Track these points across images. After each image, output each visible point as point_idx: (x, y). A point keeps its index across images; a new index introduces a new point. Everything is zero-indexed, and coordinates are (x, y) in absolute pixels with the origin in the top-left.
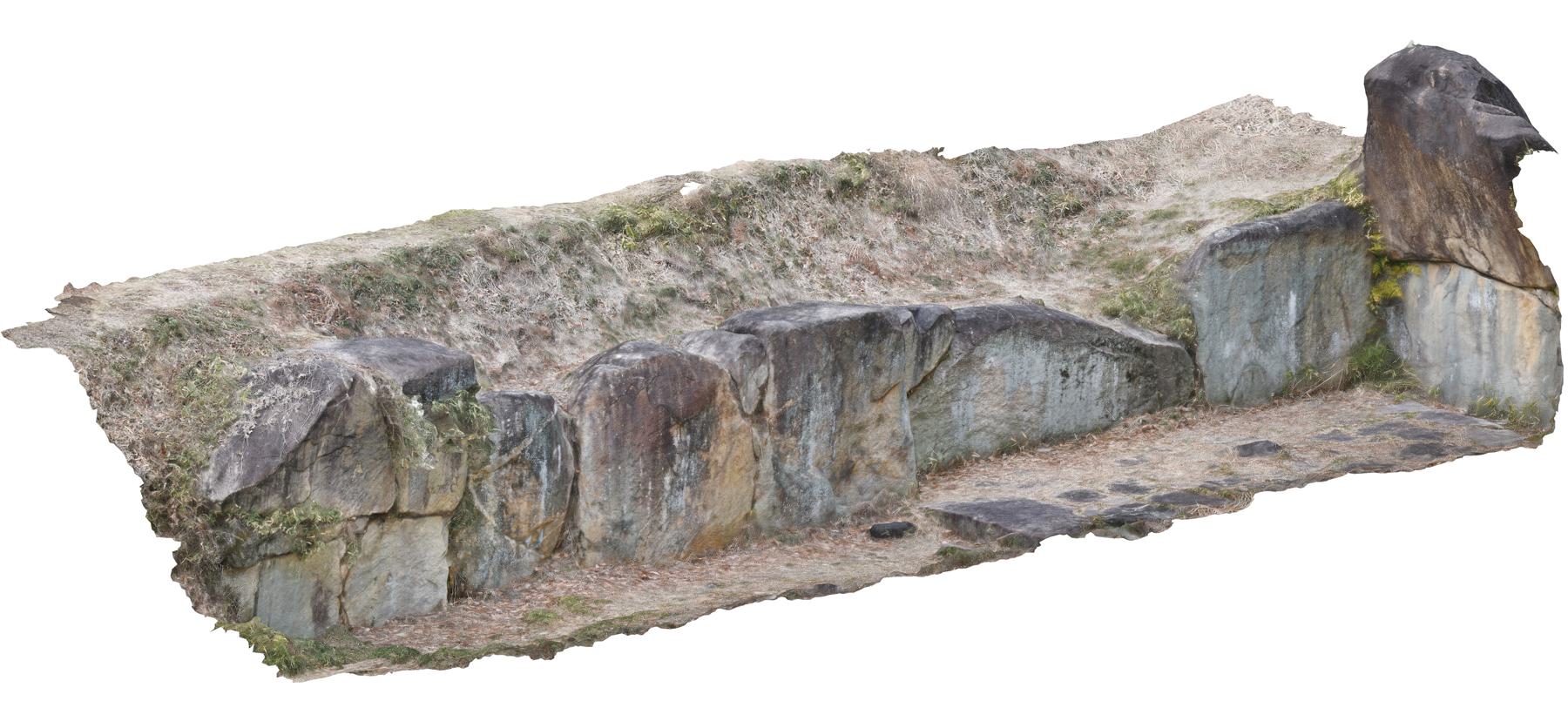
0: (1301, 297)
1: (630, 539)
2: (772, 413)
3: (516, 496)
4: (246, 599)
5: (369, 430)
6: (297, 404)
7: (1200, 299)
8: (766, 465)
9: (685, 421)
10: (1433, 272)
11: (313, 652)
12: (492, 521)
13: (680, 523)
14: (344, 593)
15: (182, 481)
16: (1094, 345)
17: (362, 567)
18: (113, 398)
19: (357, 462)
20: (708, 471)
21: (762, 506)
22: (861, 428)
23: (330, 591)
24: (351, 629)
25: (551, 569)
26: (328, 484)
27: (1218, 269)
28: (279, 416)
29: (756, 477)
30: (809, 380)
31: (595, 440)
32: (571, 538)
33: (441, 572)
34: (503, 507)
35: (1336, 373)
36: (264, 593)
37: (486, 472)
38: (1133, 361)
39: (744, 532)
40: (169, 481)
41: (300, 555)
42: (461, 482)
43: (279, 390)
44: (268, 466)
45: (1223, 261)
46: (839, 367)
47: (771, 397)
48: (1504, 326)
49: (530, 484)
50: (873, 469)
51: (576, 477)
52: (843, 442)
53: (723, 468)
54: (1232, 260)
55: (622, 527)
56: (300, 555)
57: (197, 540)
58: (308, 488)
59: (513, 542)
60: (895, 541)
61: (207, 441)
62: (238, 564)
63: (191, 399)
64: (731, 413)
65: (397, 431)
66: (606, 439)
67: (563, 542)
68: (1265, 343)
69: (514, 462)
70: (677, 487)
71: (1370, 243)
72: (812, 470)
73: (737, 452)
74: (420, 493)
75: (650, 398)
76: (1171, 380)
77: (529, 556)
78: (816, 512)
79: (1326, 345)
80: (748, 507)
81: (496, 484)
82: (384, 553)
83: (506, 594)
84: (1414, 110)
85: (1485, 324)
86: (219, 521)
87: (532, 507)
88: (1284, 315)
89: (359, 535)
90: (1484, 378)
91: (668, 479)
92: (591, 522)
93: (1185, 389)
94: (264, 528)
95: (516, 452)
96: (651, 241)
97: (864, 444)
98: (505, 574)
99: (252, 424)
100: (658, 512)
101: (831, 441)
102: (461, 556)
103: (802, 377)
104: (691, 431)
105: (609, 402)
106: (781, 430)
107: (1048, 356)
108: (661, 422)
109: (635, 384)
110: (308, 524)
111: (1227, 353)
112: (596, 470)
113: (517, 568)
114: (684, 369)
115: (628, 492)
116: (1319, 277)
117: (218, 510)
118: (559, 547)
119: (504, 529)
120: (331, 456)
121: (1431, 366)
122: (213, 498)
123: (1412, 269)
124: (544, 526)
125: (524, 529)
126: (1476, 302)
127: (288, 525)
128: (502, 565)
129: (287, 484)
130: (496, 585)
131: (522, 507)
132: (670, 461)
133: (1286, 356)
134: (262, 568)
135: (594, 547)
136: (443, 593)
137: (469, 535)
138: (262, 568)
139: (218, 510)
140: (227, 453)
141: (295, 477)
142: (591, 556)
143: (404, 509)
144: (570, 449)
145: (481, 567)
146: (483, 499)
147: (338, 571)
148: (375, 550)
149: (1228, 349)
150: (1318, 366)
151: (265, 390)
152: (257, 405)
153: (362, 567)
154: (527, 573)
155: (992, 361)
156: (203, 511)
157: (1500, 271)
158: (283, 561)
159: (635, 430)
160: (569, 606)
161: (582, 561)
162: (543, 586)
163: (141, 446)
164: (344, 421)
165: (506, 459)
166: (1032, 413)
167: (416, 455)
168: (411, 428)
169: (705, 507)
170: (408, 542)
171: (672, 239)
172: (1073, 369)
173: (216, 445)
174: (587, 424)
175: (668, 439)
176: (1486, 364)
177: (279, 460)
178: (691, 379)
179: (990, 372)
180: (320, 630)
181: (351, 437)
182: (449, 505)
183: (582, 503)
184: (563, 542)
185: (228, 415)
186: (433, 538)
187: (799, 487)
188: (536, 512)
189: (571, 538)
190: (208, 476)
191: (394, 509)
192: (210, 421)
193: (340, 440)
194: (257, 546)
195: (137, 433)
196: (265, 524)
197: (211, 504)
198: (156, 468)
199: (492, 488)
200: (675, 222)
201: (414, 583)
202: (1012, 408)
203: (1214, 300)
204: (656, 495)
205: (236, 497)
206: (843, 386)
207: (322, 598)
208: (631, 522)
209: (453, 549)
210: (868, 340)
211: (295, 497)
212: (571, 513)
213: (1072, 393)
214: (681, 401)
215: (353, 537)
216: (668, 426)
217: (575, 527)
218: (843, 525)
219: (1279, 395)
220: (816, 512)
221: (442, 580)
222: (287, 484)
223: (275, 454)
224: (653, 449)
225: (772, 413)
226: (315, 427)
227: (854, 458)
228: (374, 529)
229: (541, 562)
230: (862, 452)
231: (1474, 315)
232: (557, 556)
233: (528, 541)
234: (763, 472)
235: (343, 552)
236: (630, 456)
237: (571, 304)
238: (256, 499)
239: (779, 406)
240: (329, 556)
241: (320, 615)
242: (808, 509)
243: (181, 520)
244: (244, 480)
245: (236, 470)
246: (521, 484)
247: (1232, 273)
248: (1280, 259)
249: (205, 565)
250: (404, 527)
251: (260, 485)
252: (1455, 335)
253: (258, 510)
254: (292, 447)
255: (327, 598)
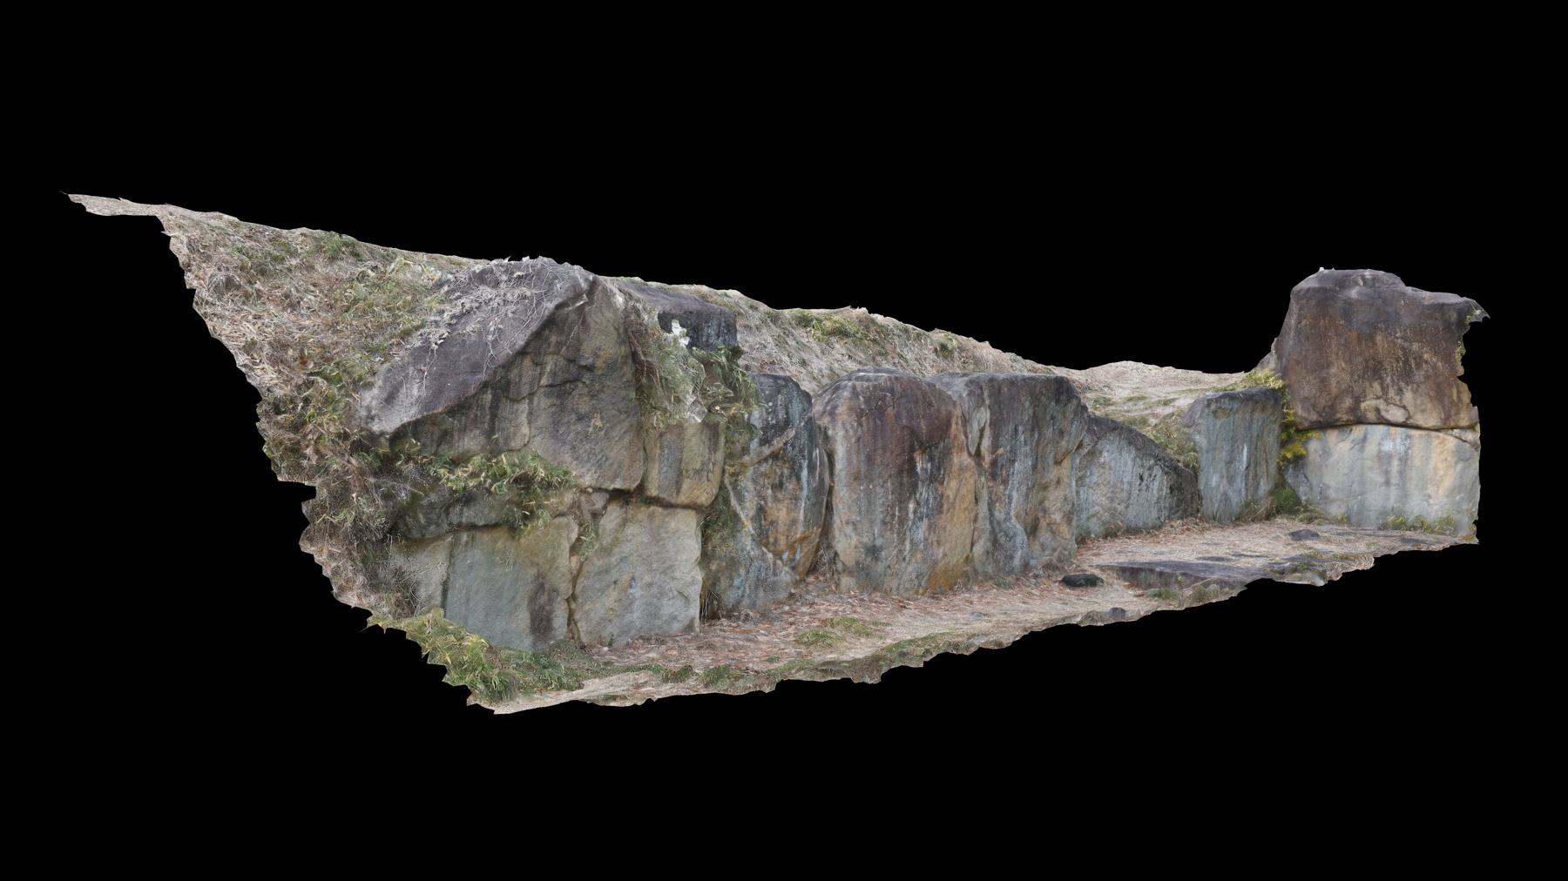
1: (880, 567)
2: (988, 458)
3: (776, 499)
5: (612, 366)
6: (512, 308)
7: (1200, 439)
8: (983, 509)
9: (927, 446)
10: (1332, 436)
11: (529, 667)
12: (749, 527)
13: (919, 556)
14: (573, 597)
15: (329, 400)
17: (599, 563)
18: (229, 284)
19: (595, 410)
20: (941, 506)
21: (979, 549)
23: (555, 590)
24: (583, 647)
25: (808, 592)
27: (1211, 418)
28: (484, 323)
29: (975, 520)
30: (1016, 431)
31: (848, 452)
32: (825, 559)
33: (693, 583)
34: (761, 510)
35: (1264, 505)
36: (458, 583)
37: (743, 466)
39: (965, 574)
40: (306, 401)
41: (513, 530)
42: (718, 470)
43: (486, 292)
44: (465, 385)
45: (1215, 412)
46: (1036, 424)
48: (1417, 462)
51: (831, 491)
52: (1034, 499)
54: (1220, 413)
55: (873, 551)
56: (513, 530)
57: (346, 488)
58: (525, 430)
59: (770, 555)
60: (1090, 589)
61: (373, 351)
62: (415, 534)
63: (356, 301)
64: (961, 450)
65: (651, 370)
66: (858, 453)
67: (817, 564)
69: (775, 456)
71: (1284, 416)
72: (1014, 520)
73: (963, 491)
74: (672, 474)
75: (898, 416)
77: (785, 576)
78: (1017, 562)
79: (1257, 488)
81: (754, 481)
82: (626, 548)
83: (764, 616)
85: (1395, 464)
86: (386, 466)
87: (791, 516)
88: (1240, 461)
89: (596, 515)
90: (1393, 501)
91: (911, 506)
92: (846, 543)
94: (455, 479)
95: (778, 443)
96: (833, 339)
97: (1047, 504)
98: (761, 594)
99: (444, 331)
100: (902, 541)
101: (1027, 495)
102: (714, 567)
103: (1011, 427)
104: (931, 459)
105: (860, 415)
108: (907, 444)
109: (883, 399)
110: (524, 481)
112: (849, 485)
113: (773, 587)
114: (925, 394)
117: (384, 449)
118: (813, 569)
119: (762, 538)
120: (561, 389)
121: (1333, 501)
122: (376, 427)
123: (1314, 434)
124: (803, 539)
125: (782, 541)
126: (1388, 446)
127: (495, 479)
128: (759, 583)
129: (494, 416)
130: (753, 606)
131: (780, 513)
132: (914, 488)
134: (454, 545)
135: (848, 571)
136: (694, 610)
137: (723, 540)
138: (454, 545)
139: (384, 449)
140: (404, 368)
141: (506, 408)
142: (846, 581)
143: (653, 491)
145: (737, 582)
146: (740, 499)
147: (567, 563)
148: (616, 542)
151: (465, 293)
152: (451, 311)
153: (599, 563)
154: (783, 595)
155: (1105, 457)
156: (359, 447)
157: (1419, 419)
158: (486, 537)
160: (847, 628)
161: (837, 585)
162: (804, 609)
163: (267, 349)
164: (579, 342)
165: (767, 451)
167: (678, 400)
168: (670, 362)
169: (939, 543)
170: (656, 538)
171: (849, 340)
173: (387, 357)
174: (841, 433)
176: (1394, 493)
177: (483, 377)
178: (930, 405)
180: (542, 646)
181: (590, 368)
182: (704, 498)
183: (837, 521)
184: (817, 564)
185: (407, 321)
186: (684, 533)
187: (1006, 535)
188: (794, 522)
189: (825, 559)
190: (370, 398)
191: (641, 488)
192: (381, 327)
193: (573, 369)
194: (447, 508)
195: (261, 331)
196: (459, 472)
197: (374, 438)
198: (287, 382)
199: (750, 486)
200: (851, 329)
201: (662, 594)
202: (1112, 501)
204: (902, 521)
205: (414, 428)
207: (543, 599)
208: (881, 548)
209: (706, 557)
210: (1058, 401)
211: (507, 440)
212: (826, 530)
213: (1144, 494)
214: (923, 425)
215: (588, 516)
216: (912, 450)
217: (829, 547)
218: (1036, 576)
219: (1238, 519)
220: (1017, 562)
221: (695, 592)
222: (494, 416)
223: (475, 368)
224: (900, 472)
225: (988, 458)
226: (537, 335)
228: (613, 515)
229: (797, 584)
231: (1383, 458)
232: (811, 579)
233: (785, 556)
234: (981, 515)
235: (574, 536)
236: (880, 476)
237: (785, 358)
238: (445, 436)
239: (993, 452)
240: (553, 536)
241: (541, 625)
242: (1012, 557)
243: (322, 456)
244: (427, 404)
245: (415, 391)
247: (1218, 422)
249: (359, 530)
250: (651, 516)
251: (452, 412)
252: (1362, 475)
253: (449, 453)
254: (501, 359)
255: (551, 600)
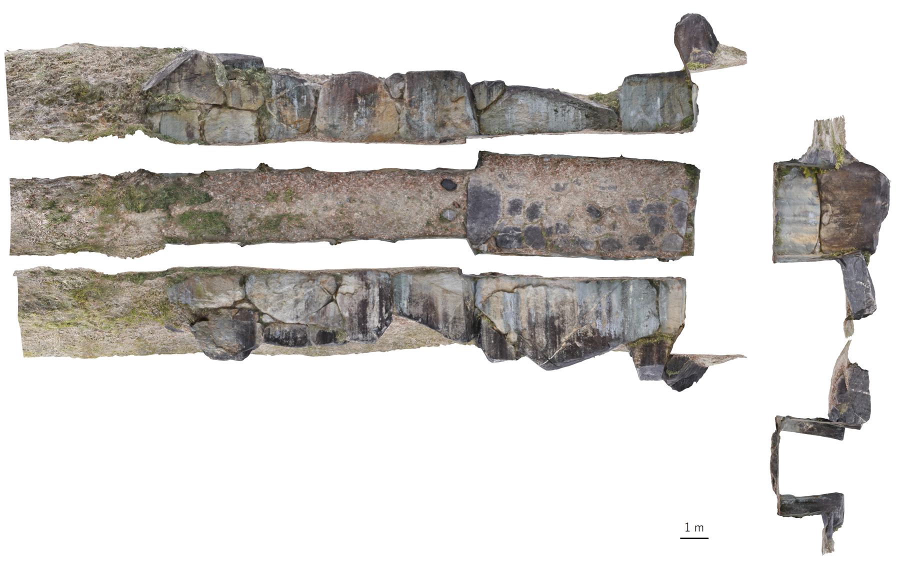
0: (662, 99)
1: (337, 131)
2: (407, 99)
4: (156, 125)
9: (363, 95)
16: (568, 103)
21: (402, 130)
22: (447, 110)
26: (189, 89)
30: (422, 90)
31: (324, 97)
36: (163, 124)
38: (587, 111)
47: (406, 94)
49: (290, 105)
50: (454, 125)
51: (316, 108)
53: (382, 114)
64: (386, 96)
68: (648, 114)
69: (282, 97)
70: (360, 116)
76: (606, 120)
79: (675, 117)
80: (396, 130)
84: (875, 200)
86: (146, 98)
91: (355, 114)
93: (613, 124)
95: (282, 93)
105: (332, 86)
106: (410, 106)
107: (548, 104)
111: (630, 114)
112: (324, 107)
115: (337, 115)
116: (669, 93)
119: (281, 119)
131: (288, 113)
132: (357, 108)
133: (657, 119)
141: (171, 84)
144: (313, 98)
146: (271, 109)
149: (632, 113)
150: (670, 124)
155: (520, 101)
156: (141, 94)
159: (342, 96)
166: (543, 123)
170: (235, 117)
172: (560, 110)
175: (356, 101)
179: (521, 105)
183: (317, 117)
203: (625, 96)
204: (350, 118)
205: (151, 90)
206: (437, 94)
213: (560, 118)
214: (361, 89)
216: (356, 96)
224: (349, 103)
225: (407, 99)
227: (446, 120)
228: (215, 111)
230: (449, 119)
246: (286, 105)
247: (633, 88)
248: (652, 85)
